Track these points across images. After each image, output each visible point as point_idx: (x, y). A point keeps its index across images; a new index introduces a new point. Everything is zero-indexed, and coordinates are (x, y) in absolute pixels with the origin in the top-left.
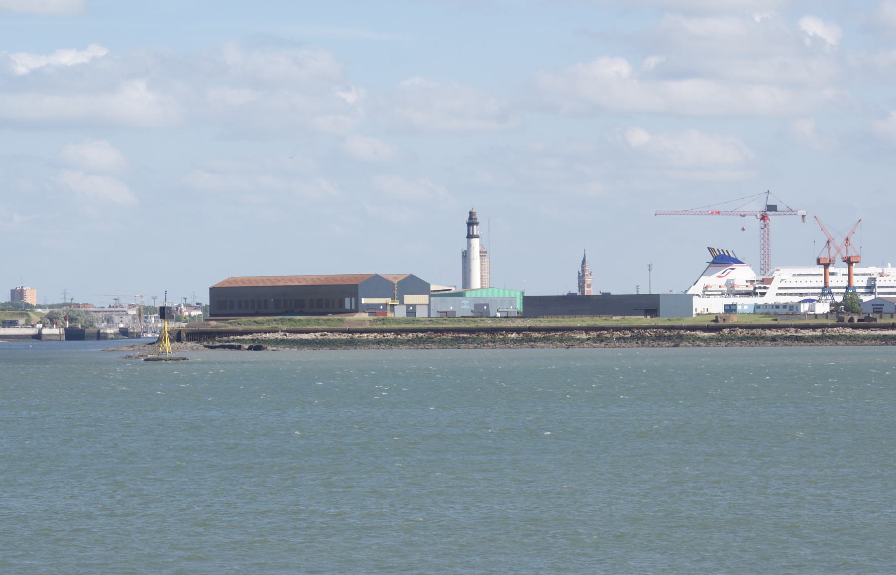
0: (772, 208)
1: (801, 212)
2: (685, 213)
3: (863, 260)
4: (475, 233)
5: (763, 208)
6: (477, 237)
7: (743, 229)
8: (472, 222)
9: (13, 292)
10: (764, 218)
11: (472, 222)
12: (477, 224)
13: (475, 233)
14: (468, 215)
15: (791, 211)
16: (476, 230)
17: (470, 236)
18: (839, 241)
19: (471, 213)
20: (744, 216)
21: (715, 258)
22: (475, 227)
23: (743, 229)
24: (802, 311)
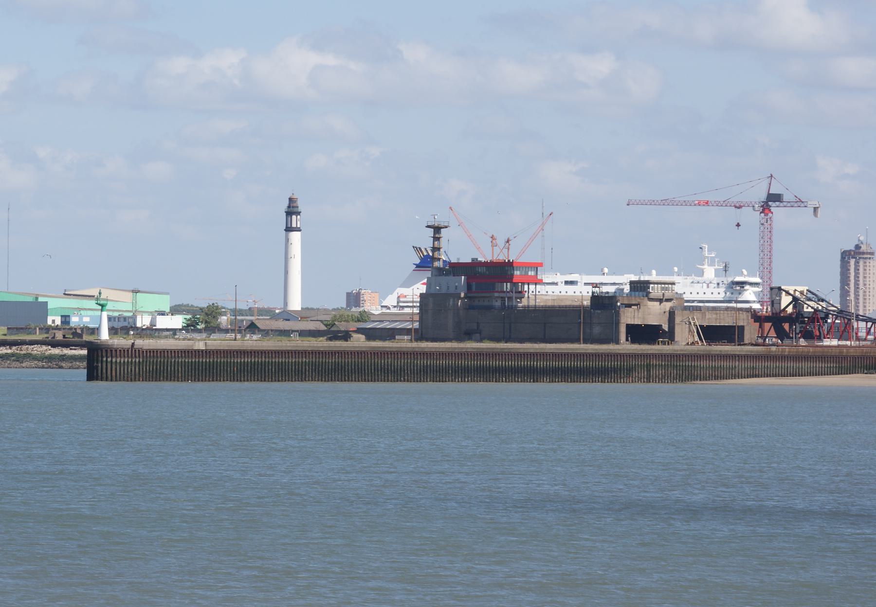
0: (776, 198)
1: (813, 203)
2: (665, 202)
3: (547, 264)
4: (294, 225)
5: (763, 197)
6: (298, 229)
7: (738, 225)
8: (292, 210)
9: (349, 295)
10: (765, 208)
11: (292, 210)
12: (298, 213)
13: (294, 225)
14: (287, 203)
15: (799, 202)
16: (295, 221)
17: (289, 229)
18: (501, 242)
19: (290, 199)
20: (740, 207)
21: (421, 259)
22: (294, 217)
23: (738, 225)
24: (49, 322)
